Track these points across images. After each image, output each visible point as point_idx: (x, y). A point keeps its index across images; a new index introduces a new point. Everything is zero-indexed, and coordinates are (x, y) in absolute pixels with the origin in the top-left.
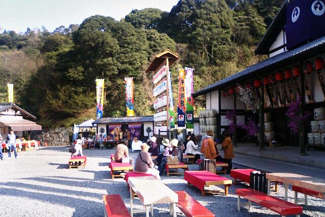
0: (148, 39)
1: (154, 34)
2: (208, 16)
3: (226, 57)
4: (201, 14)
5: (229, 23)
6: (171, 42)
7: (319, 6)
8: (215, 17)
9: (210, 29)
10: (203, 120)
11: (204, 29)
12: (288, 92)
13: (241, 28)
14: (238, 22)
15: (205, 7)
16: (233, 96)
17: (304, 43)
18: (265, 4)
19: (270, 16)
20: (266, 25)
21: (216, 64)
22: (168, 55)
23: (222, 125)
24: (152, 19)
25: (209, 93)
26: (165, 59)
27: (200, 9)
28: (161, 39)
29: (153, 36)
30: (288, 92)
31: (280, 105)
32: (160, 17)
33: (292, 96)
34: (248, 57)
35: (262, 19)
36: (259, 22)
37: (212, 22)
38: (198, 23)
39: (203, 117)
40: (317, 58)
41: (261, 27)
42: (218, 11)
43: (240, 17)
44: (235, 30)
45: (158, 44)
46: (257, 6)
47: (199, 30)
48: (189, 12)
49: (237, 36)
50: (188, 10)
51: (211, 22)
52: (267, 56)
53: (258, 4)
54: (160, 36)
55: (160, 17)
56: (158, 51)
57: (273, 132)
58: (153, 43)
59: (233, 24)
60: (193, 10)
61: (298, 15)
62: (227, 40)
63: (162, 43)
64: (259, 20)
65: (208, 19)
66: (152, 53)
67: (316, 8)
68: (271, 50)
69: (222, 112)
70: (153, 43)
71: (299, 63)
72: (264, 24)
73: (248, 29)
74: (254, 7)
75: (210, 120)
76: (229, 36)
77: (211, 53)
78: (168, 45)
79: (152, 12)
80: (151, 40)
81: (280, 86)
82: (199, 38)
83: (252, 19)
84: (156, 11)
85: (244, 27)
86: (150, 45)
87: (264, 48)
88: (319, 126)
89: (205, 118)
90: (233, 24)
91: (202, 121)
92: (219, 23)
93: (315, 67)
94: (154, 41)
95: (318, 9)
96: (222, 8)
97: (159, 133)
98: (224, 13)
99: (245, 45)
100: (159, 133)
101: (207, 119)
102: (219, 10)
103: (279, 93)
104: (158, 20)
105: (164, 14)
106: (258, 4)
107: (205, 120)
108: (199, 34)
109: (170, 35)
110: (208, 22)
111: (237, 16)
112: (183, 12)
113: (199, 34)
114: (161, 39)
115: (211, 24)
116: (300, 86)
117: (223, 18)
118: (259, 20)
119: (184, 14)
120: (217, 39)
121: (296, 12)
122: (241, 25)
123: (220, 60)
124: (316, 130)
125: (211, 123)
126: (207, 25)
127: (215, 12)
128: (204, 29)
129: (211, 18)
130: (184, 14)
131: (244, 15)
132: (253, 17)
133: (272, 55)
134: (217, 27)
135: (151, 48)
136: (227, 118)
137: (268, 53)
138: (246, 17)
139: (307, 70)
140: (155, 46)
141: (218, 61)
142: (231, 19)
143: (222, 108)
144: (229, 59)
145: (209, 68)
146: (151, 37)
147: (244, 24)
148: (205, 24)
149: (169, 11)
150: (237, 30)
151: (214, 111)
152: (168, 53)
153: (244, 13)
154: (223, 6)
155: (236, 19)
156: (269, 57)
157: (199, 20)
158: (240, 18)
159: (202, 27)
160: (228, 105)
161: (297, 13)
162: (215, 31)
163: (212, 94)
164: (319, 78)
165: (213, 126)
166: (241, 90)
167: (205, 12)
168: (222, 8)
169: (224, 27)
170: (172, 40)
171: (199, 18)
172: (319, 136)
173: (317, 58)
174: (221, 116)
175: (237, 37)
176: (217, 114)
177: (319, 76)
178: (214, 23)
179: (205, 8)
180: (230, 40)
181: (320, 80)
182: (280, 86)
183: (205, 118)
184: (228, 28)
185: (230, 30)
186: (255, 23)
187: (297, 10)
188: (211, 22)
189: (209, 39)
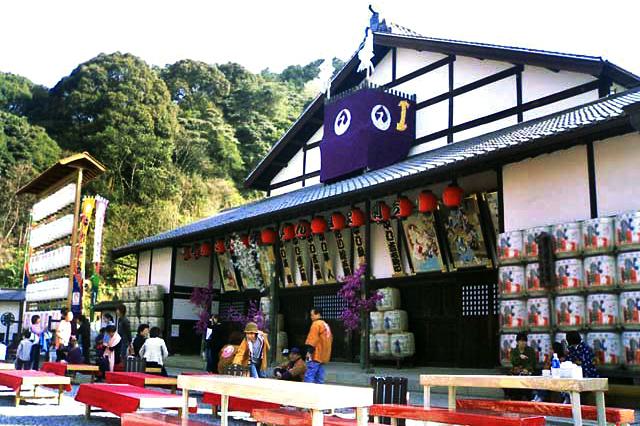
0: (6, 131)
1: (20, 125)
2: (132, 108)
3: (159, 190)
4: (117, 99)
5: (170, 128)
6: (51, 146)
7: (382, 114)
8: (145, 111)
9: (132, 132)
10: (133, 305)
11: (121, 130)
12: (320, 257)
13: (191, 140)
14: (187, 128)
15: (126, 89)
16: (208, 260)
17: (358, 173)
18: (238, 104)
19: (247, 126)
20: (237, 142)
21: (140, 202)
22: (83, 162)
23: (174, 317)
24: (12, 94)
25: (149, 252)
26: (76, 170)
27: (116, 91)
28: (33, 137)
29: (18, 128)
30: (320, 257)
31: (299, 282)
32: (30, 95)
33: (328, 266)
34: (201, 196)
35: (232, 131)
36: (226, 134)
37: (138, 120)
38: (109, 117)
39: (133, 299)
40: (424, 192)
41: (230, 144)
42: (151, 102)
43: (192, 119)
44: (180, 143)
45: (27, 144)
46: (222, 106)
47: (110, 130)
48: (95, 93)
49: (183, 154)
50: (93, 89)
51: (137, 119)
52: (265, 193)
53: (226, 101)
54: (31, 131)
55: (30, 95)
56: (27, 158)
57: (404, 312)
58: (14, 140)
59: (177, 131)
60: (102, 91)
61: (348, 123)
62: (164, 159)
63: (34, 145)
64: (227, 131)
65: (129, 113)
66: (13, 160)
67: (377, 116)
68: (275, 181)
69: (177, 291)
70: (14, 140)
71: (210, 240)
72: (236, 140)
73: (204, 144)
74: (217, 105)
75: (151, 306)
76: (169, 151)
77: (129, 182)
78: (46, 148)
79: (12, 81)
80: (10, 135)
81: (303, 245)
82: (110, 146)
83: (214, 128)
84: (22, 81)
85: (198, 140)
86: (9, 143)
87: (259, 179)
88: (387, 320)
89: (138, 301)
90: (177, 131)
91: (130, 308)
92: (151, 124)
93: (398, 212)
94: (19, 138)
95: (380, 119)
96: (159, 97)
97: (50, 324)
98: (162, 107)
99: (198, 173)
100: (50, 324)
101: (143, 304)
102: (154, 101)
103: (300, 260)
104: (22, 99)
105: (38, 91)
106: (226, 101)
107: (138, 307)
108: (109, 139)
109: (50, 132)
110: (129, 118)
111: (185, 116)
112: (82, 92)
113: (110, 140)
114: (33, 137)
115: (134, 123)
116: (347, 249)
117: (159, 116)
118: (227, 131)
119: (84, 97)
120: (144, 154)
121: (343, 117)
122: (193, 136)
123: (148, 195)
124: (379, 329)
125: (152, 314)
126: (126, 123)
127: (144, 102)
128: (121, 130)
129: (137, 112)
130: (84, 97)
131: (198, 118)
132: (216, 124)
133: (274, 193)
134: (147, 132)
135: (10, 149)
136: (192, 301)
137: (269, 188)
138: (202, 122)
139: (380, 217)
140: (20, 148)
141: (143, 196)
142: (175, 121)
143: (176, 284)
144: (166, 195)
145: (124, 207)
146: (13, 129)
147: (196, 133)
148: (123, 121)
149: (50, 84)
150: (185, 144)
151: (160, 288)
152: (84, 159)
153: (199, 113)
154: (161, 93)
155: (182, 123)
156: (269, 195)
157: (111, 113)
158: (190, 122)
159: (116, 126)
160: (194, 277)
161: (346, 119)
162: (144, 138)
163: (155, 251)
164: (387, 236)
165: (156, 319)
166: (238, 246)
167: (125, 98)
168: (159, 97)
169: (160, 133)
170: (54, 143)
171: (113, 108)
172: (386, 340)
173: (335, 213)
174: (175, 300)
175: (183, 156)
176: (166, 295)
177: (387, 233)
178: (141, 122)
179: (126, 92)
180: (170, 160)
181: (388, 239)
182: (303, 245)
183: (138, 301)
184: (168, 137)
185: (171, 140)
186: (219, 135)
187: (344, 114)
188: (137, 119)
189: (129, 152)
